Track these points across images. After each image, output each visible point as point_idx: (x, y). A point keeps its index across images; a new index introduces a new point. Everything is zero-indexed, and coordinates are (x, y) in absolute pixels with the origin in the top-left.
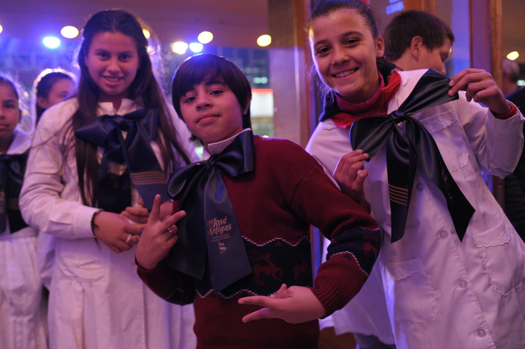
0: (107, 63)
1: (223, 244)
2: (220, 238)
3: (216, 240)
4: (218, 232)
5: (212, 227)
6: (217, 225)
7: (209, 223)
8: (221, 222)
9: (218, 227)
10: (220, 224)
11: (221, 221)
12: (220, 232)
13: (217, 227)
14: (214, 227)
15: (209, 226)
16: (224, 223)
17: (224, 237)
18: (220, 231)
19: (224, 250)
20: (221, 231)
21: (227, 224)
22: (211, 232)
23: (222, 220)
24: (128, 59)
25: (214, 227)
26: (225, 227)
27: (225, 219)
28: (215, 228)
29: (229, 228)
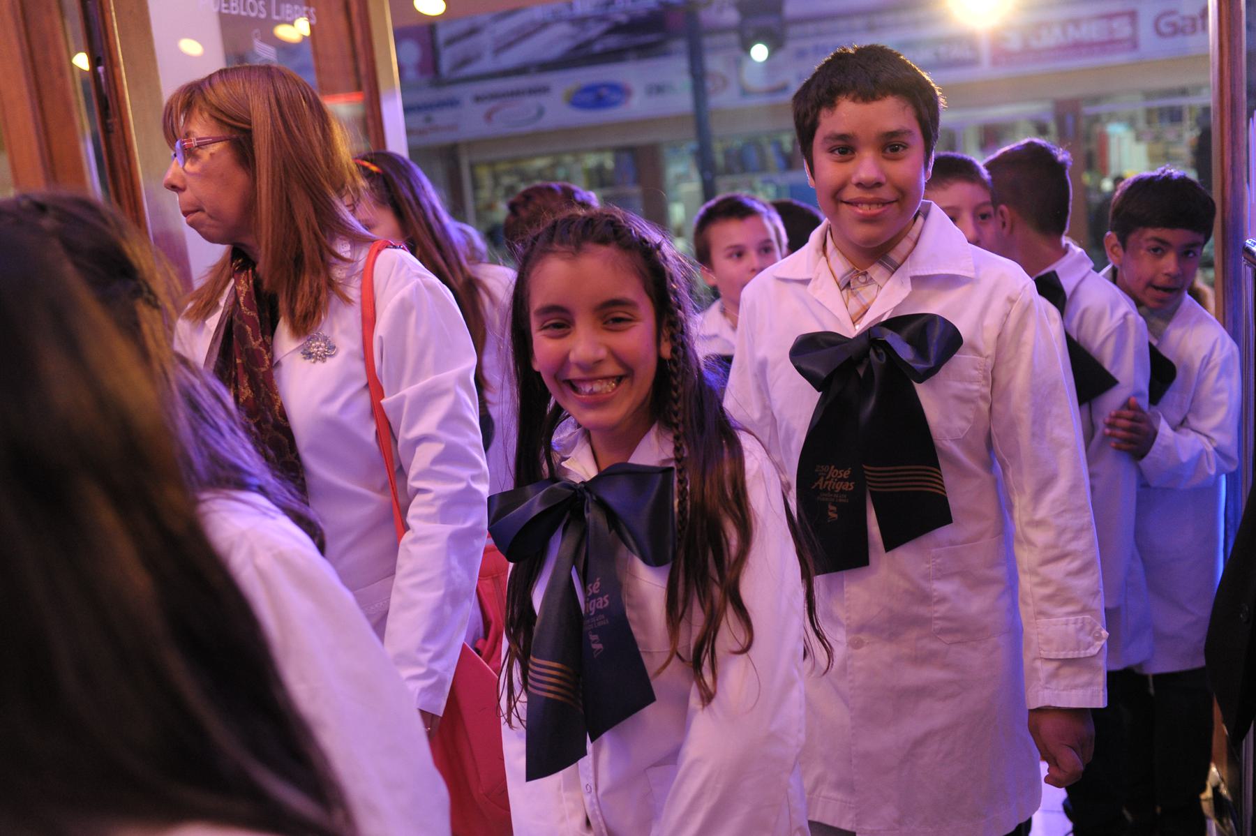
0: (848, 168)
1: (834, 508)
2: (833, 497)
3: (827, 499)
4: (833, 488)
5: (825, 477)
6: (833, 476)
7: (821, 469)
8: (841, 475)
9: (834, 481)
10: (839, 477)
11: (840, 472)
12: (835, 489)
13: (832, 479)
14: (827, 478)
15: (820, 474)
16: (845, 477)
17: (838, 498)
18: (835, 487)
19: (834, 518)
20: (837, 487)
21: (849, 480)
22: (821, 484)
23: (843, 471)
24: (901, 153)
25: (827, 478)
26: (597, 601)
27: (597, 585)
28: (829, 480)
29: (849, 487)
